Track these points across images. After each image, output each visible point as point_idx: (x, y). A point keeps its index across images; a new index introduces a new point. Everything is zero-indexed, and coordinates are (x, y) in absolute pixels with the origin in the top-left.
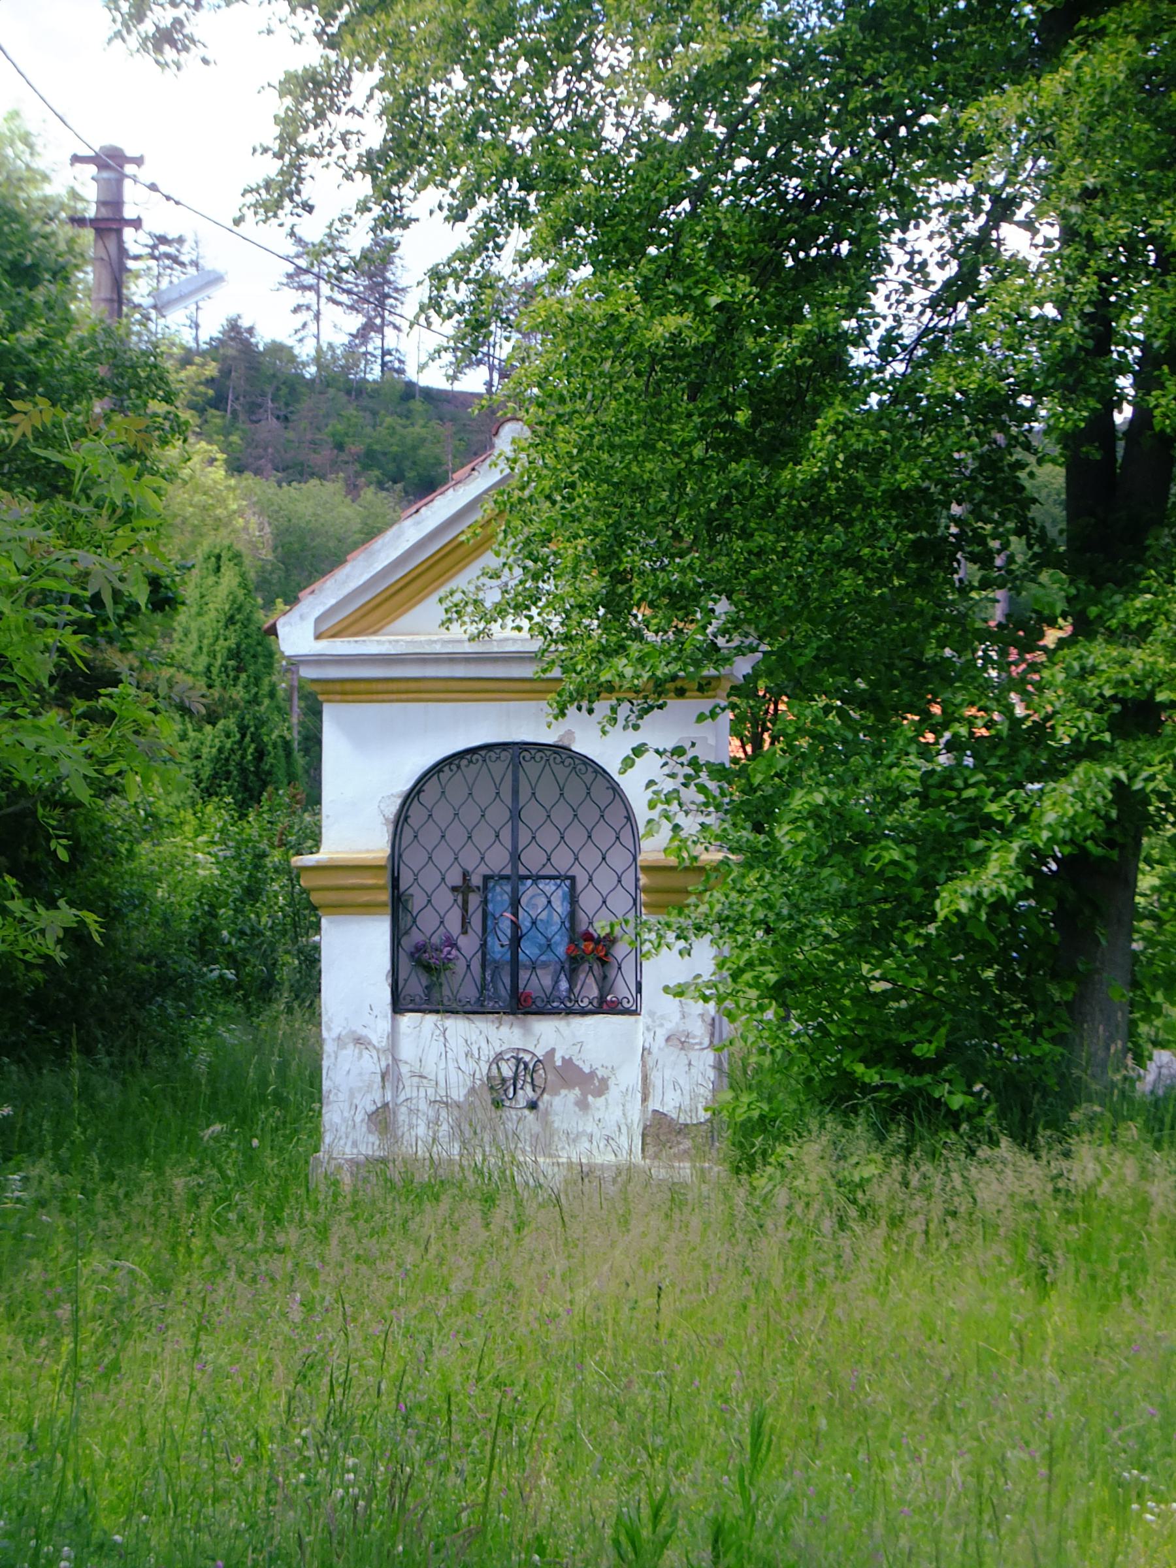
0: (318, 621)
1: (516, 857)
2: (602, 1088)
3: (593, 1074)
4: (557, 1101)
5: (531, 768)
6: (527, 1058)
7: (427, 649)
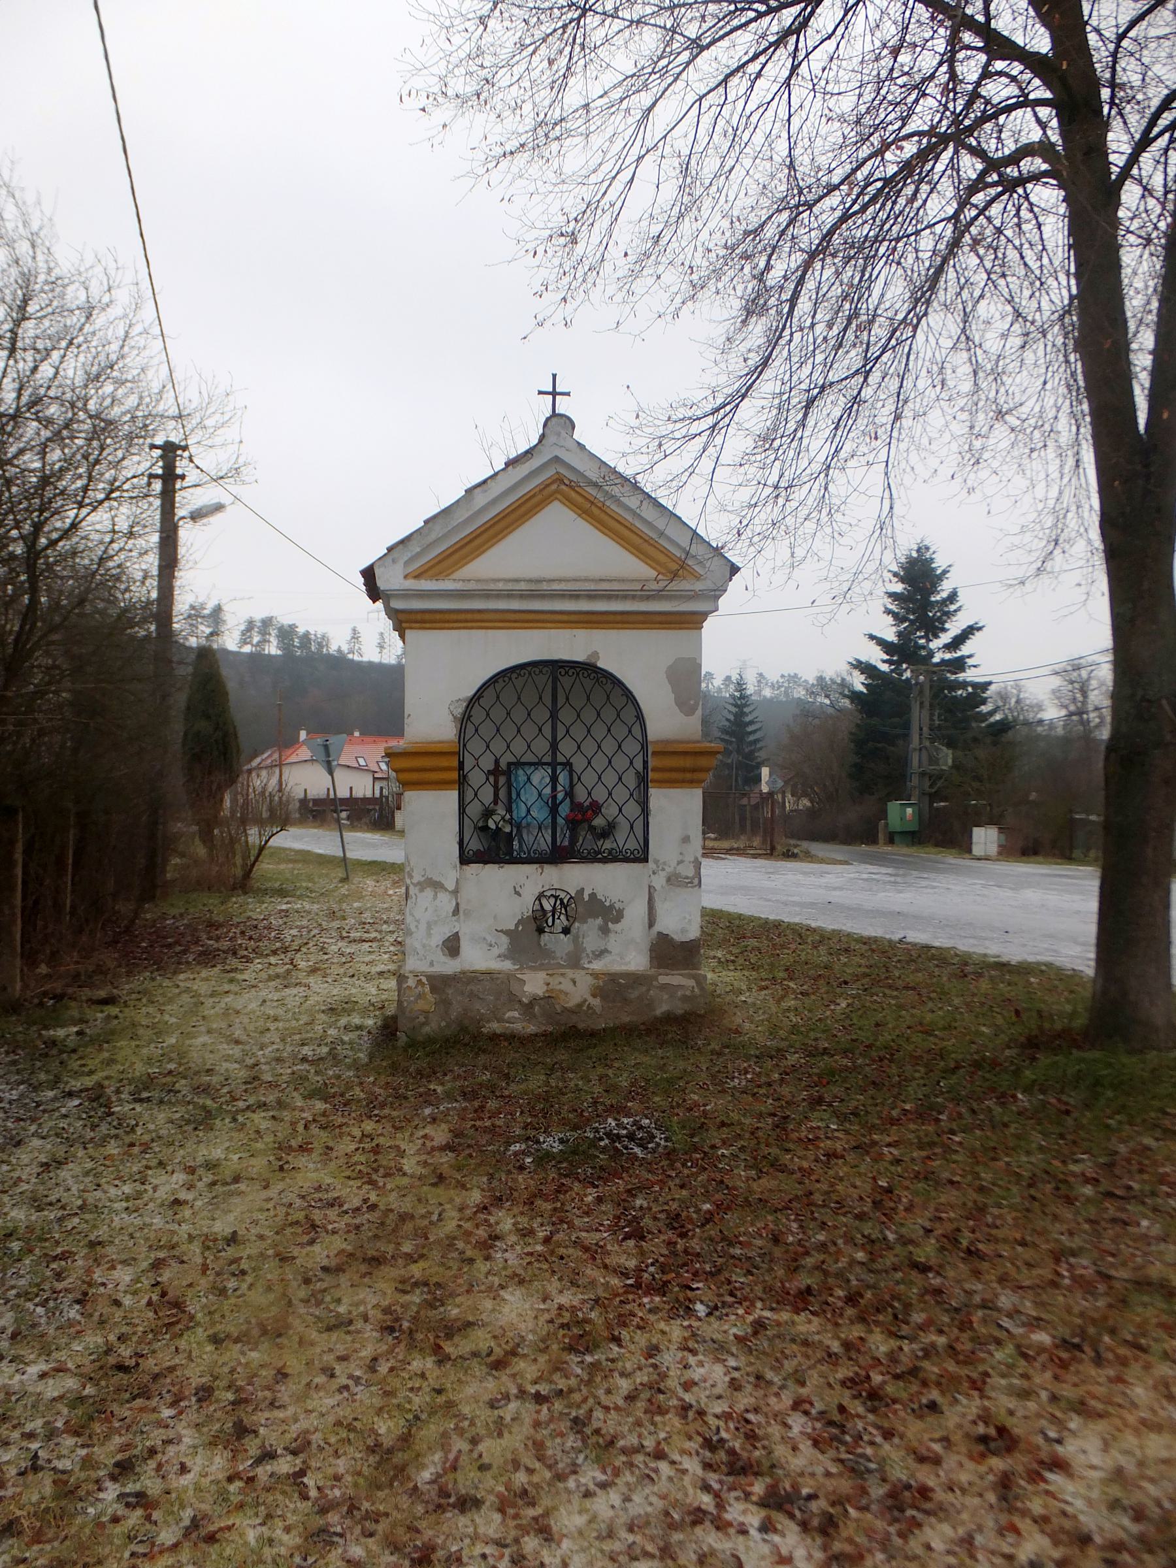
0: (406, 563)
1: (554, 746)
2: (618, 916)
3: (612, 907)
4: (585, 927)
5: (566, 681)
6: (562, 895)
7: (492, 586)
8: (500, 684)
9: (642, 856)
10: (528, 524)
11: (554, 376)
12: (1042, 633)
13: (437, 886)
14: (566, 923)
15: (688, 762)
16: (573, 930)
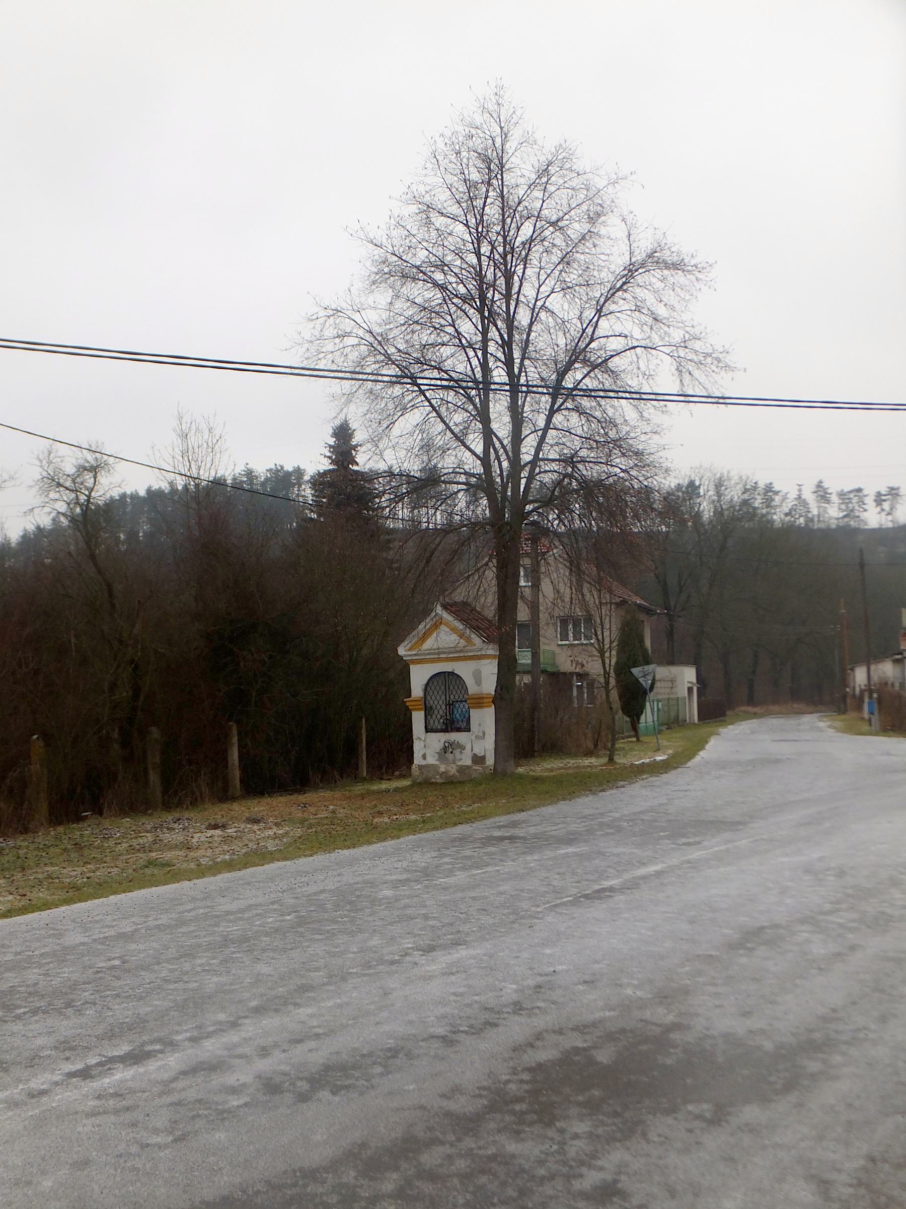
9: (468, 730)
13: (420, 739)
15: (476, 701)
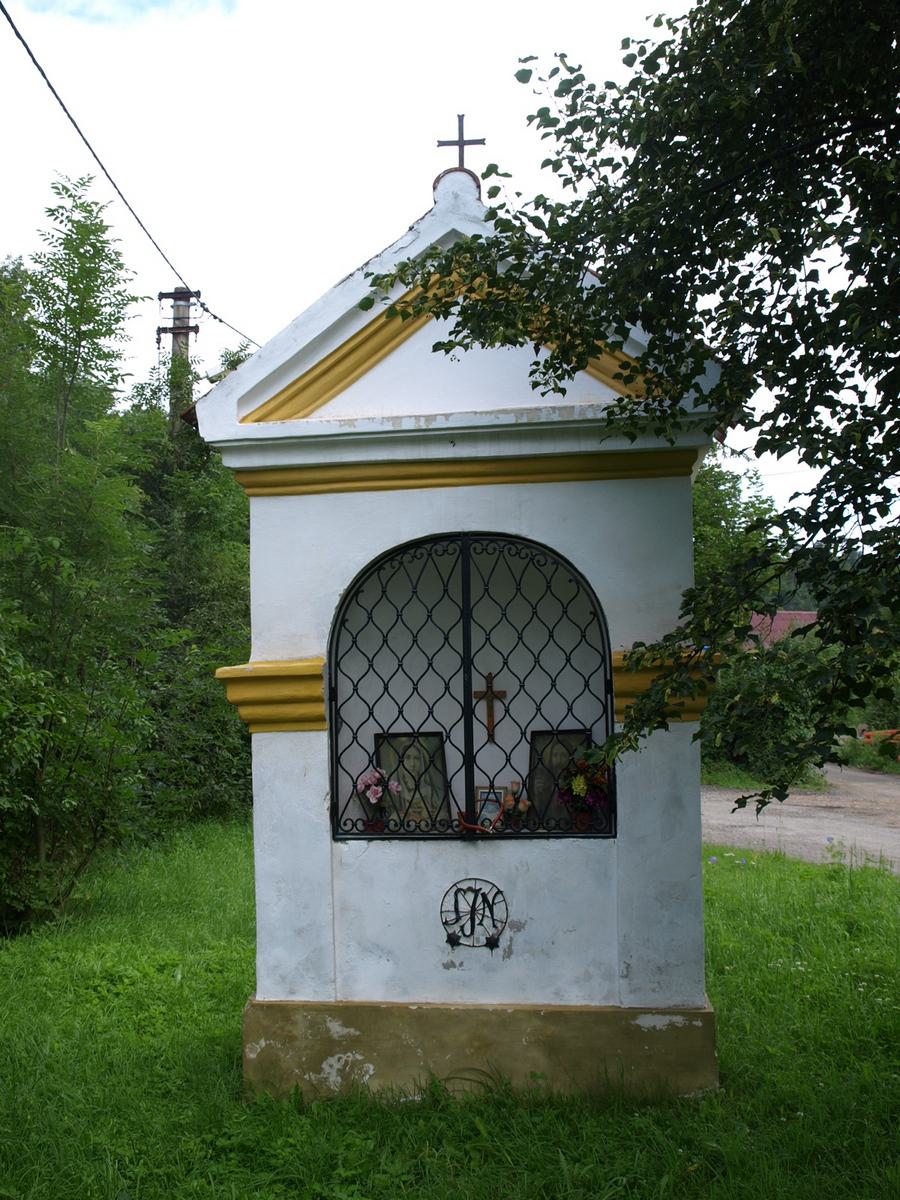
6: (486, 889)
8: (387, 571)
10: (292, 734)
11: (461, 118)
12: (839, 434)
14: (492, 931)
16: (503, 942)
